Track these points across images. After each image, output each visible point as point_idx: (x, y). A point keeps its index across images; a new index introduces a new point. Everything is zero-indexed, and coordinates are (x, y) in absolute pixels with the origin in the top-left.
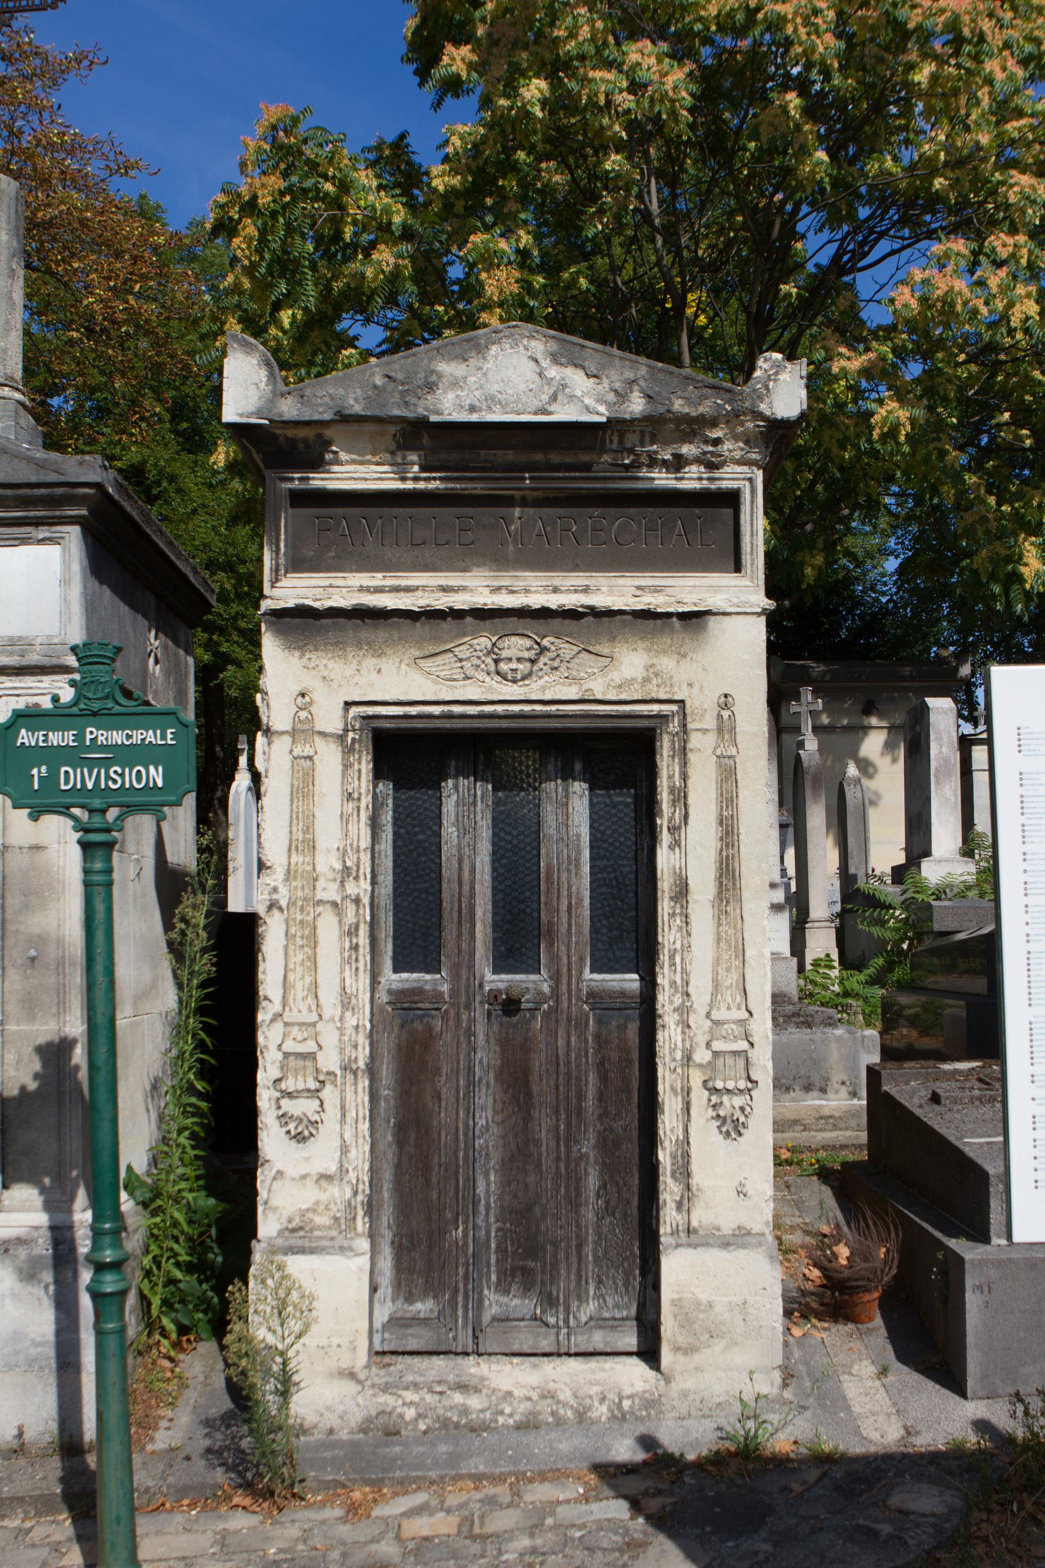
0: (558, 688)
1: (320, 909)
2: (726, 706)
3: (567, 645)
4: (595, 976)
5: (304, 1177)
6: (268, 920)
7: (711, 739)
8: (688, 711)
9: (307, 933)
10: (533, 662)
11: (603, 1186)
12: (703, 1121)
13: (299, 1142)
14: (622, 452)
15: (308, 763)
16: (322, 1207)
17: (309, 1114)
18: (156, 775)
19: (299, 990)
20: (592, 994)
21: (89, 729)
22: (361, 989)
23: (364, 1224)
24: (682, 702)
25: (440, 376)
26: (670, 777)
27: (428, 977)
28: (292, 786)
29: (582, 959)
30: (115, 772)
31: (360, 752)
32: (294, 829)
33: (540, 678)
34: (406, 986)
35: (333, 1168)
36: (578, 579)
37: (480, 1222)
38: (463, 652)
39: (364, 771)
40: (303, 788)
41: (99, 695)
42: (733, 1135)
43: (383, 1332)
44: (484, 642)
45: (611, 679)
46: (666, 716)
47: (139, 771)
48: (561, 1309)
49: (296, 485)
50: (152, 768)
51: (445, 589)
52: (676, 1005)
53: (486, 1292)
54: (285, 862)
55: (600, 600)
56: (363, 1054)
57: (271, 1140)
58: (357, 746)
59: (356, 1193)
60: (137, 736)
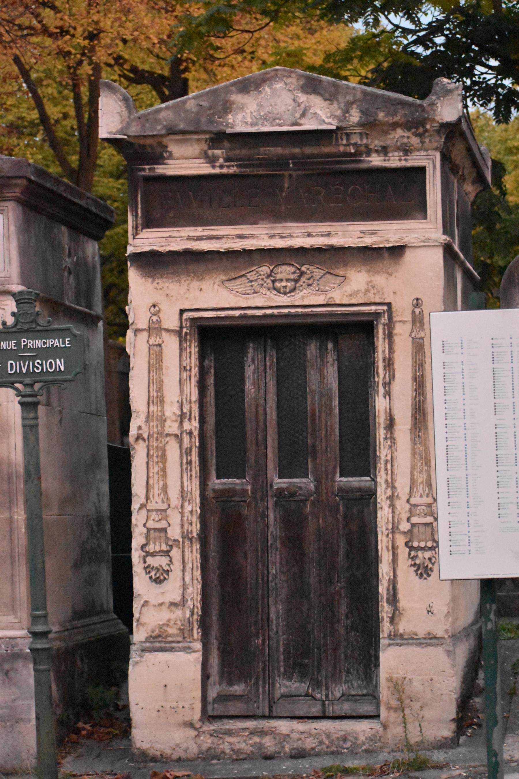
0: (312, 297)
1: (167, 439)
2: (417, 305)
3: (317, 270)
4: (343, 479)
5: (161, 604)
6: (136, 447)
7: (408, 327)
8: (394, 309)
9: (160, 454)
10: (296, 281)
11: (350, 612)
12: (405, 567)
13: (157, 583)
14: (349, 145)
15: (158, 348)
16: (172, 623)
17: (164, 566)
18: (60, 364)
19: (156, 490)
20: (340, 490)
21: (23, 340)
22: (194, 488)
23: (198, 633)
24: (389, 305)
25: (233, 103)
26: (384, 352)
27: (238, 481)
28: (149, 363)
29: (335, 468)
30: (38, 363)
31: (190, 341)
32: (151, 390)
33: (301, 291)
34: (227, 487)
35: (177, 598)
36: (324, 227)
37: (272, 634)
38: (252, 276)
39: (193, 352)
40: (156, 364)
41: (28, 320)
42: (425, 576)
43: (213, 703)
44: (265, 270)
45: (349, 290)
46: (380, 314)
47: (51, 363)
48: (324, 688)
49: (147, 173)
50: (58, 361)
51: (241, 237)
52: (388, 495)
53: (277, 678)
54: (146, 410)
55: (336, 241)
56: (196, 528)
57: (141, 583)
58: (188, 337)
59: (192, 614)
60: (50, 343)
